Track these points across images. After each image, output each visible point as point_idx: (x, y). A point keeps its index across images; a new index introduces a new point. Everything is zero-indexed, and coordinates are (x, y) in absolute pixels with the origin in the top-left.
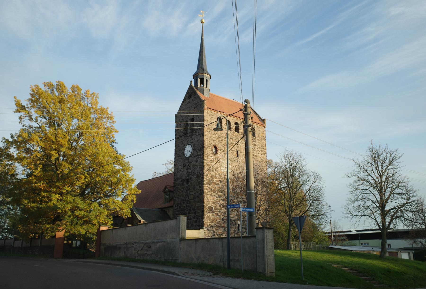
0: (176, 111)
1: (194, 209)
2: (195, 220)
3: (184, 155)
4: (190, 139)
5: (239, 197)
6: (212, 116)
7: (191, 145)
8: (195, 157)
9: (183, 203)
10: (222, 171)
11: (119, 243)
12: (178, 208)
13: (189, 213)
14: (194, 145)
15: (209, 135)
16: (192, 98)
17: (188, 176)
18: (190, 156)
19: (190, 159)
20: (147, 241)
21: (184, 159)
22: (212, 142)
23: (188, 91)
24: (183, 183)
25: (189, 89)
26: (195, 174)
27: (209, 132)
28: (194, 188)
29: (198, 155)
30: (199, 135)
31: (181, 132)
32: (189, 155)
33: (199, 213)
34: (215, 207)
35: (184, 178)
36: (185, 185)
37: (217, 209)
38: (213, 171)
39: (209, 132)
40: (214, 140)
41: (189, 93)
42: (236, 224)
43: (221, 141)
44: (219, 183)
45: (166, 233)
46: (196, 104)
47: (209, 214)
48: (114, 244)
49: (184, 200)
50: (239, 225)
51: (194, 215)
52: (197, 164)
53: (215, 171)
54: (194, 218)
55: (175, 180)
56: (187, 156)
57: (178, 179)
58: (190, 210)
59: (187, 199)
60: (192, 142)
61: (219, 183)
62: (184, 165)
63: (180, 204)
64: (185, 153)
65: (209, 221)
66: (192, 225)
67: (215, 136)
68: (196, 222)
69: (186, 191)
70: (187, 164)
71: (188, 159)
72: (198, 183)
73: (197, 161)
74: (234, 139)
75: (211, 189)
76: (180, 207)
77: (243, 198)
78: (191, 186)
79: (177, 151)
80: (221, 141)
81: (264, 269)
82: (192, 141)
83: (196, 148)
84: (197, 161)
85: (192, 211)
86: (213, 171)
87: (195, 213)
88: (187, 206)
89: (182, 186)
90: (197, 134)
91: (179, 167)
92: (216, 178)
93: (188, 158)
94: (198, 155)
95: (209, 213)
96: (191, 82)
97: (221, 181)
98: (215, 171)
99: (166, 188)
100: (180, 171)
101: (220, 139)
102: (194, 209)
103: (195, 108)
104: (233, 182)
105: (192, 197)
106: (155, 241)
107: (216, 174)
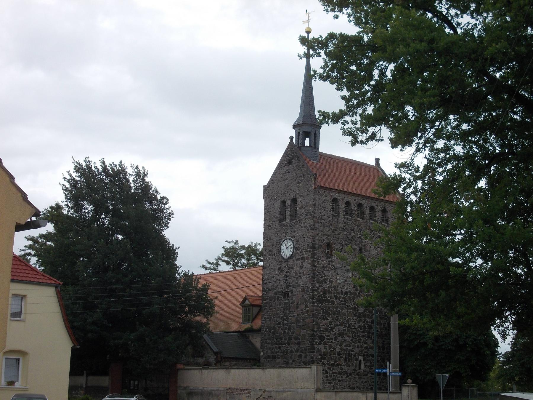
0: (266, 183)
1: (296, 339)
2: (299, 353)
3: (279, 253)
4: (289, 231)
5: (361, 320)
6: (325, 198)
7: (292, 241)
8: (298, 259)
9: (279, 327)
10: (338, 281)
11: (216, 389)
12: (269, 335)
13: (288, 343)
14: (298, 241)
15: (322, 228)
16: (294, 165)
17: (287, 287)
18: (291, 257)
19: (291, 262)
20: (268, 389)
21: (280, 260)
22: (324, 238)
23: (286, 151)
24: (278, 297)
25: (288, 149)
26: (299, 286)
27: (321, 223)
28: (297, 307)
29: (303, 258)
30: (306, 227)
31: (274, 216)
32: (288, 256)
33: (305, 344)
34: (327, 336)
35: (279, 289)
36: (282, 300)
37: (332, 339)
38: (325, 282)
39: (321, 223)
40: (328, 236)
41: (288, 156)
42: (357, 360)
43: (337, 236)
44: (334, 299)
45: (296, 382)
46: (301, 177)
47: (320, 346)
48: (205, 389)
49: (279, 324)
50: (361, 361)
51: (297, 346)
52: (302, 271)
53: (328, 282)
54: (297, 350)
55: (264, 290)
56: (285, 257)
57: (269, 290)
58: (290, 339)
59: (285, 322)
60: (294, 237)
61: (334, 299)
62: (280, 270)
63: (274, 328)
64: (282, 251)
65: (320, 357)
66: (294, 361)
67: (329, 228)
68: (300, 356)
69: (284, 310)
70: (285, 269)
71: (287, 262)
72: (303, 301)
73: (303, 267)
74: (356, 230)
75: (323, 310)
76: (273, 333)
77: (367, 322)
78: (293, 303)
79: (268, 246)
80: (337, 236)
81: (259, 297)
82: (294, 234)
83: (300, 246)
84: (301, 267)
85: (293, 340)
86: (325, 282)
87: (299, 344)
88: (284, 332)
89: (278, 302)
90: (302, 225)
91: (272, 271)
92: (330, 293)
93: (287, 260)
94: (303, 258)
95: (319, 344)
96: (292, 138)
97: (336, 298)
98: (328, 282)
99: (245, 299)
100: (273, 277)
101: (336, 233)
102: (296, 339)
103: (298, 183)
104: (354, 298)
105: (293, 319)
106: (280, 390)
107: (330, 287)
